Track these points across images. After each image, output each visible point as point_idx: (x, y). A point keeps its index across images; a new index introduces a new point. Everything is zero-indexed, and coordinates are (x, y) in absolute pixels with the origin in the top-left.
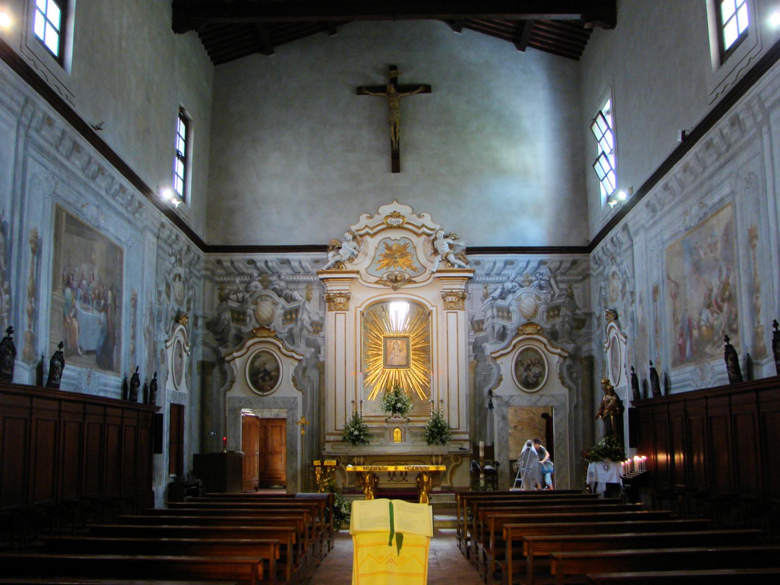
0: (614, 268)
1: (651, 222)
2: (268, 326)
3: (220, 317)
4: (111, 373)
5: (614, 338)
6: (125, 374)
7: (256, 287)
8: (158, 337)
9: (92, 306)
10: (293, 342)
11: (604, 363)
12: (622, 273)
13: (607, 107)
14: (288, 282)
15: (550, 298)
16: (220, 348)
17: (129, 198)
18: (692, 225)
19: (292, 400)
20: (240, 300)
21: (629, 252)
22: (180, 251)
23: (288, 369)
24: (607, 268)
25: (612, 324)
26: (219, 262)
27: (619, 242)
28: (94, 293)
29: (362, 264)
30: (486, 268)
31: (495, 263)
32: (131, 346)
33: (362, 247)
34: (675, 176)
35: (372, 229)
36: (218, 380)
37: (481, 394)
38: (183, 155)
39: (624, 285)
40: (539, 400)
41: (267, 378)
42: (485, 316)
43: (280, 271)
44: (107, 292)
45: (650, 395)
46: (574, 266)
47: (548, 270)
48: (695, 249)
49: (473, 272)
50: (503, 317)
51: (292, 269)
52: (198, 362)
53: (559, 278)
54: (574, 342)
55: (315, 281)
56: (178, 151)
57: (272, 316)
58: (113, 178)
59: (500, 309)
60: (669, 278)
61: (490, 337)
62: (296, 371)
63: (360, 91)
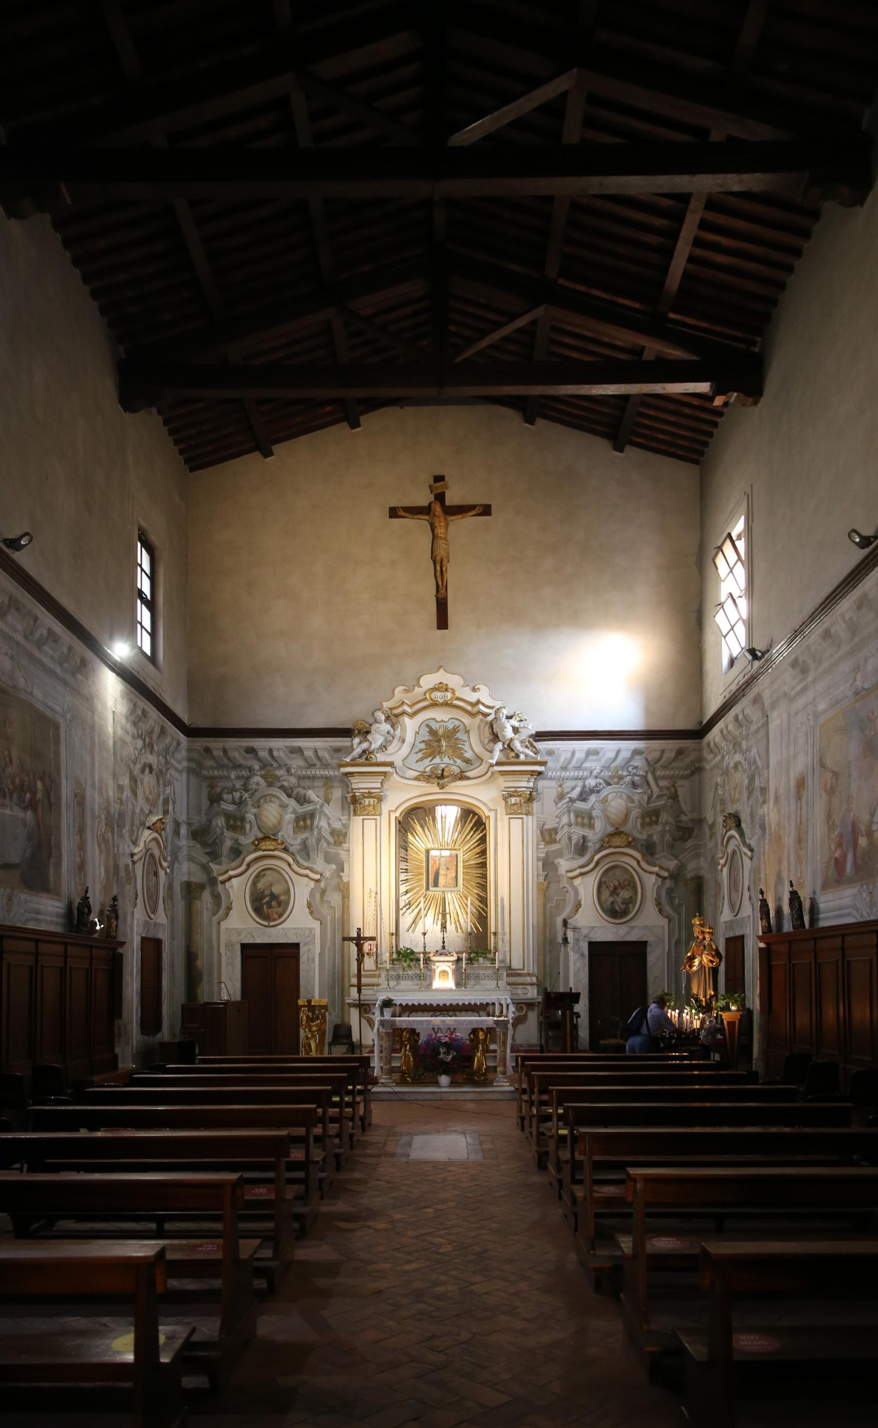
0: (738, 757)
1: (798, 688)
2: (274, 835)
3: (210, 826)
4: (45, 895)
5: (734, 852)
6: (69, 898)
7: (258, 784)
8: (121, 847)
9: (11, 800)
10: (308, 857)
11: (718, 885)
12: (749, 764)
13: (739, 527)
14: (300, 778)
15: (646, 799)
16: (211, 864)
17: (65, 650)
18: (866, 687)
19: (308, 932)
20: (237, 801)
21: (762, 733)
22: (150, 733)
23: (301, 891)
24: (727, 758)
25: (733, 832)
26: (207, 750)
27: (747, 720)
28: (13, 783)
29: (397, 754)
30: (562, 760)
31: (573, 753)
32: (78, 859)
33: (398, 732)
34: (843, 616)
35: (411, 706)
36: (209, 906)
37: (553, 925)
38: (149, 598)
39: (752, 780)
40: (628, 933)
41: (274, 903)
42: (559, 823)
43: (288, 762)
44: (36, 783)
45: (787, 927)
46: (680, 757)
47: (644, 761)
48: (869, 720)
49: (543, 764)
50: (583, 825)
51: (306, 760)
52: (181, 884)
53: (658, 773)
54: (676, 857)
55: (336, 776)
56: (140, 593)
57: (279, 823)
58: (36, 619)
59: (578, 814)
60: (822, 765)
61: (565, 851)
62: (312, 893)
63: (394, 513)
